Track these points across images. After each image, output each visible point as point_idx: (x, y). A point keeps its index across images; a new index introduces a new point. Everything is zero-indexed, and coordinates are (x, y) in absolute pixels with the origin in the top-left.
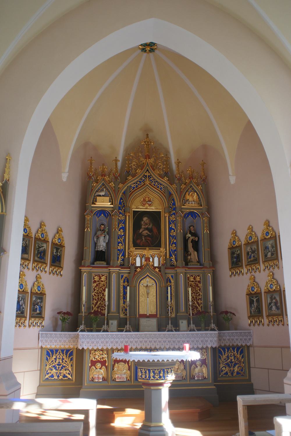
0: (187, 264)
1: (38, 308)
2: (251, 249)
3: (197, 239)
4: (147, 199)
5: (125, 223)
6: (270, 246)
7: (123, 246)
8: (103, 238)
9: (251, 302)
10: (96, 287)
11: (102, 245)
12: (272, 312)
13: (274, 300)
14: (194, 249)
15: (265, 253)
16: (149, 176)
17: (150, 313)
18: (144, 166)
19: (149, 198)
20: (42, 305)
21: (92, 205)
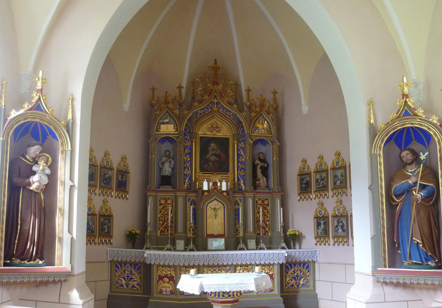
0: (255, 188)
1: (106, 228)
2: (321, 176)
3: (266, 165)
4: (215, 126)
5: (191, 148)
6: (339, 174)
7: (190, 171)
8: (168, 163)
9: (319, 224)
10: (162, 209)
11: (167, 170)
12: (338, 234)
13: (341, 224)
14: (263, 175)
15: (334, 181)
16: (217, 103)
17: (218, 233)
18: (211, 93)
19: (216, 125)
20: (109, 225)
21: (156, 133)
